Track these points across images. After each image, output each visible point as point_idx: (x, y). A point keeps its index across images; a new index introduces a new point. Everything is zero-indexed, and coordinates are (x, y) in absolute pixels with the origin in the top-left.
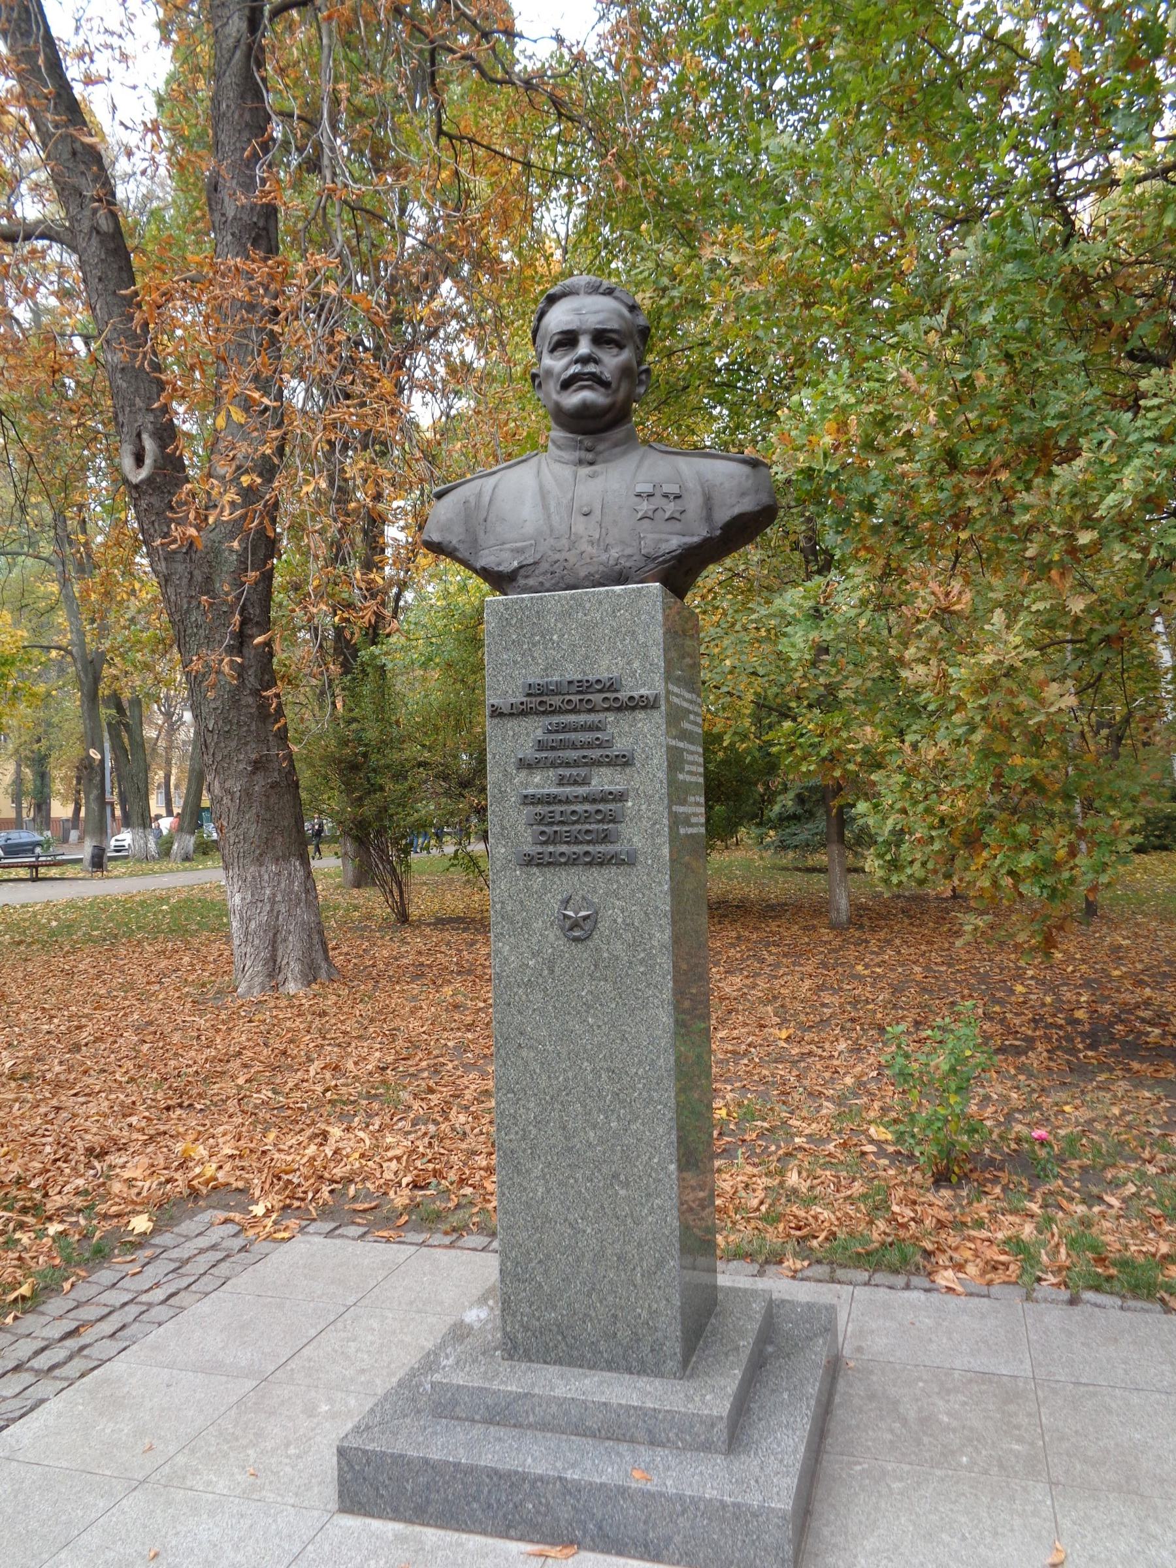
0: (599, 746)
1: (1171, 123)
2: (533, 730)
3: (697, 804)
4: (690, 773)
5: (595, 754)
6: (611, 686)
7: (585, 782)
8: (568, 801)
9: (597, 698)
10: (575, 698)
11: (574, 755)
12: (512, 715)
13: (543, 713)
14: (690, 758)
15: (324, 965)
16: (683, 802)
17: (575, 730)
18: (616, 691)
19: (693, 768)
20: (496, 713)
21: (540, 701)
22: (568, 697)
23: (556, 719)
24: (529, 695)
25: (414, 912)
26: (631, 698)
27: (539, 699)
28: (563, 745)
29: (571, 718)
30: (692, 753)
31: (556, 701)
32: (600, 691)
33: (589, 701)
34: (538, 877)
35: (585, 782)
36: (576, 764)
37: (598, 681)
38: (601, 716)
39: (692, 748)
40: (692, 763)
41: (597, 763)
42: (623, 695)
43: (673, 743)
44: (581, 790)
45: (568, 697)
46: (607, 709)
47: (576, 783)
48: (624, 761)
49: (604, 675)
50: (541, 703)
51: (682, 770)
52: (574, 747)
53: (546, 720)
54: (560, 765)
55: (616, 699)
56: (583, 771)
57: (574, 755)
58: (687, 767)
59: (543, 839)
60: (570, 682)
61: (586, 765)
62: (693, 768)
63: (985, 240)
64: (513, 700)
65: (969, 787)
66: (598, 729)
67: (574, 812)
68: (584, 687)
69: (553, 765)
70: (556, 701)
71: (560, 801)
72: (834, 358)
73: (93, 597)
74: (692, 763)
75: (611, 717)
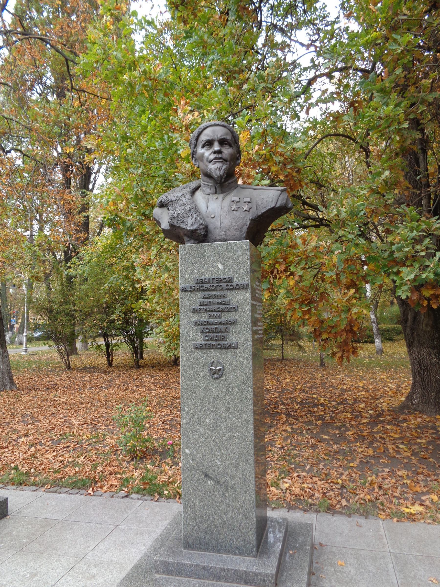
0: (224, 304)
2: (199, 297)
5: (223, 307)
6: (230, 280)
7: (219, 317)
8: (213, 324)
10: (215, 285)
11: (215, 307)
12: (190, 291)
15: (9, 385)
17: (215, 298)
20: (184, 290)
21: (201, 286)
22: (212, 285)
23: (207, 293)
24: (197, 283)
25: (73, 365)
27: (201, 285)
28: (210, 304)
29: (214, 293)
31: (207, 286)
33: (221, 286)
34: (198, 354)
35: (219, 317)
36: (215, 310)
37: (225, 279)
38: (225, 292)
41: (223, 311)
42: (234, 284)
43: (253, 302)
44: (219, 320)
45: (212, 285)
46: (228, 289)
47: (216, 317)
48: (235, 310)
49: (227, 277)
50: (202, 286)
51: (256, 313)
52: (214, 304)
53: (203, 293)
54: (209, 311)
55: (231, 285)
56: (218, 314)
57: (215, 307)
58: (258, 311)
59: (207, 338)
60: (213, 279)
61: (219, 311)
63: (149, 118)
66: (224, 297)
67: (207, 329)
68: (219, 281)
69: (206, 311)
70: (207, 286)
71: (210, 324)
75: (229, 293)
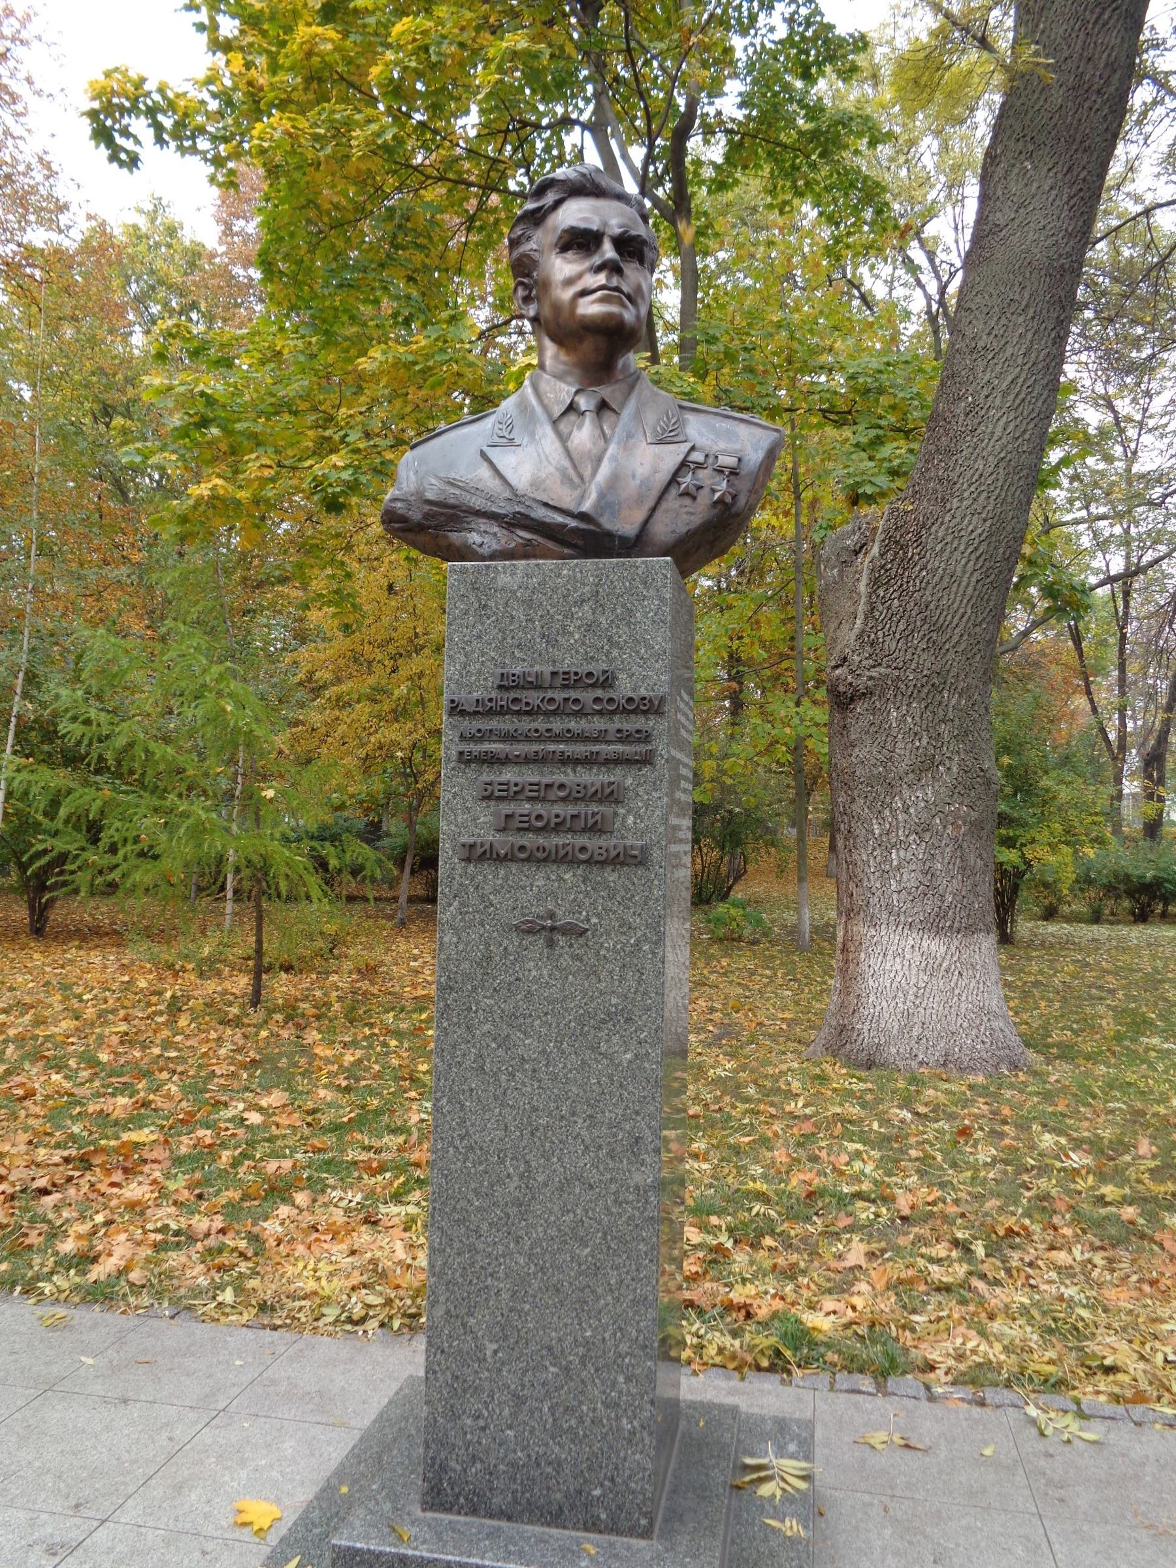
9: (587, 696)
13: (518, 713)
24: (500, 687)
30: (685, 765)
68: (571, 681)
70: (534, 698)
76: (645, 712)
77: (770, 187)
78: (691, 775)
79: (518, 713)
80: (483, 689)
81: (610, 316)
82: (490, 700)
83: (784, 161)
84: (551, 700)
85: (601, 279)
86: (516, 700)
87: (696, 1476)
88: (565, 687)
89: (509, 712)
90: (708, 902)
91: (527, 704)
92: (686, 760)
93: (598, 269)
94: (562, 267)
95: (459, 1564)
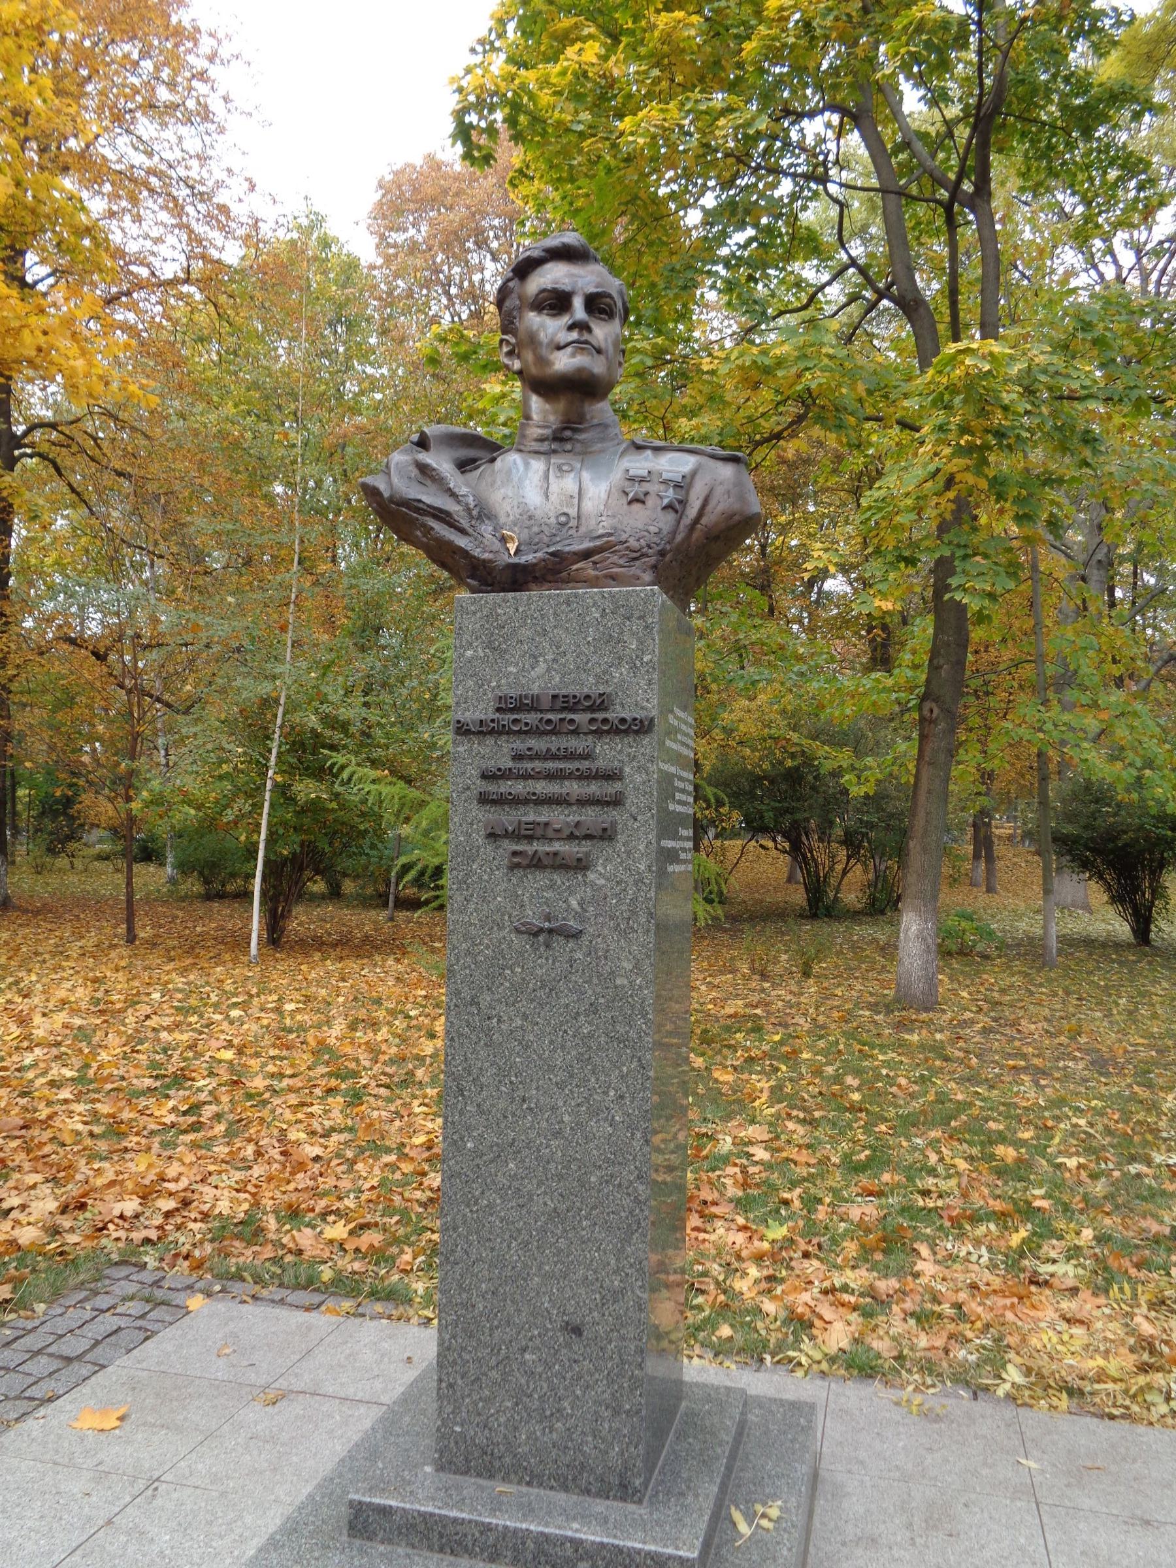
1: (1165, 223)
3: (688, 839)
4: (680, 802)
6: (600, 704)
9: (581, 718)
13: (520, 732)
14: (681, 785)
16: (675, 836)
18: (606, 709)
19: (684, 797)
24: (498, 710)
26: (623, 721)
30: (681, 779)
32: (587, 709)
33: (572, 721)
37: (588, 697)
39: (684, 774)
40: (683, 791)
42: (614, 714)
49: (595, 691)
55: (605, 721)
62: (684, 797)
64: (483, 717)
65: (301, 1122)
68: (569, 704)
70: (531, 718)
72: (315, 428)
73: (1147, 323)
74: (683, 791)
76: (637, 732)
77: (1023, 169)
78: (691, 788)
79: (520, 732)
80: (481, 711)
81: (580, 370)
82: (493, 721)
83: (1039, 141)
84: (549, 721)
85: (574, 335)
86: (515, 721)
87: (657, 1442)
88: (563, 709)
89: (510, 732)
90: (882, 912)
91: (527, 724)
92: (684, 774)
93: (571, 328)
94: (550, 327)
95: (653, 1556)
